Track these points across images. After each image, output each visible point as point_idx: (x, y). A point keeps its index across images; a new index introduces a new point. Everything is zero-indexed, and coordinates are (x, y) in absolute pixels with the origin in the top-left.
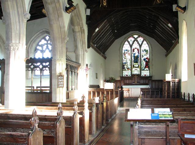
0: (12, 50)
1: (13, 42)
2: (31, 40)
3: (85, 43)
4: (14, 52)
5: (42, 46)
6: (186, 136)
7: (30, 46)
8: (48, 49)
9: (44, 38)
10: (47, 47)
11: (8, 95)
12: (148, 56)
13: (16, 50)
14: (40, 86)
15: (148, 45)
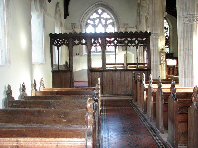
2: (85, 13)
3: (178, 17)
5: (94, 20)
7: (83, 20)
8: (102, 23)
9: (96, 12)
10: (100, 22)
12: (168, 34)
14: (115, 63)
15: (168, 23)
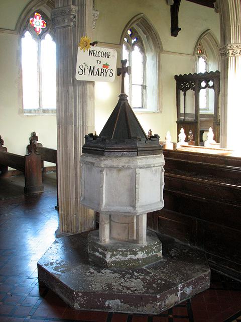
0: (230, 55)
1: (233, 41)
4: (234, 58)
6: (160, 217)
11: (225, 128)
13: (238, 54)
14: (37, 107)
